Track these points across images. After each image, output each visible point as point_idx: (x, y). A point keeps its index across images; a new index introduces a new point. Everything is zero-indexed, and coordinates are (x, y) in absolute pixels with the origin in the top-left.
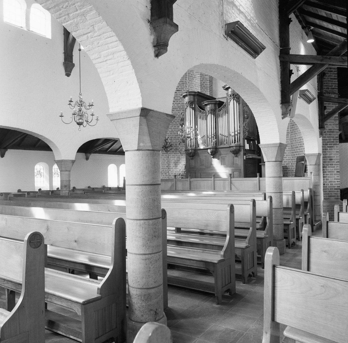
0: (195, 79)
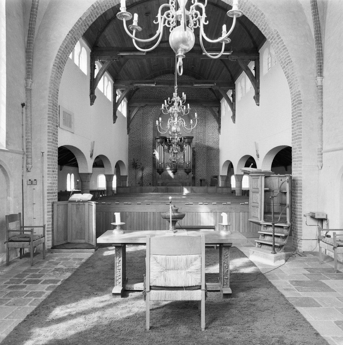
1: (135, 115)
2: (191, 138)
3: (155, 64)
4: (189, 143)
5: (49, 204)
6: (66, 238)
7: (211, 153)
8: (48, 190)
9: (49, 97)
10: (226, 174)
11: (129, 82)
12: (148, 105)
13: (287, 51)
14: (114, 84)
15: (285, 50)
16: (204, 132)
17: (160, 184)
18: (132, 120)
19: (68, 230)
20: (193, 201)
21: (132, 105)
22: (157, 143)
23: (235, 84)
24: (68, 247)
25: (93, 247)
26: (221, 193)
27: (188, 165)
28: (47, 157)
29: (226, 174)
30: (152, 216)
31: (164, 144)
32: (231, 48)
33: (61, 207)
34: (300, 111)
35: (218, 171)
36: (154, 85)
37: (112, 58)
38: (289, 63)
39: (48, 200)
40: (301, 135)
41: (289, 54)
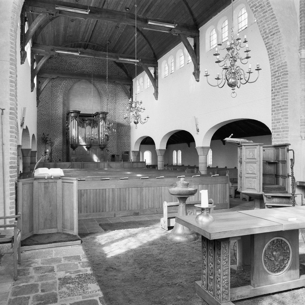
0: (58, 98)
1: (44, 87)
2: (105, 114)
3: (70, 35)
4: (104, 119)
5: (12, 183)
6: (32, 229)
7: (122, 130)
8: (11, 163)
9: (11, 30)
10: (138, 150)
11: (51, 47)
12: (59, 77)
13: (276, 20)
14: (31, 48)
15: (273, 20)
16: (115, 109)
17: (74, 160)
18: (42, 92)
19: (34, 218)
20: (110, 176)
21: (42, 76)
22: (70, 118)
23: (158, 63)
24: (45, 242)
25: (75, 238)
26: (142, 168)
27: (102, 141)
28: (10, 117)
29: (138, 150)
30: (111, 193)
31: (78, 118)
32: (174, 21)
33: (27, 187)
34: (286, 82)
35: (129, 146)
36: (78, 54)
37: (48, 12)
38: (276, 33)
39: (11, 177)
40: (287, 105)
41: (277, 24)
